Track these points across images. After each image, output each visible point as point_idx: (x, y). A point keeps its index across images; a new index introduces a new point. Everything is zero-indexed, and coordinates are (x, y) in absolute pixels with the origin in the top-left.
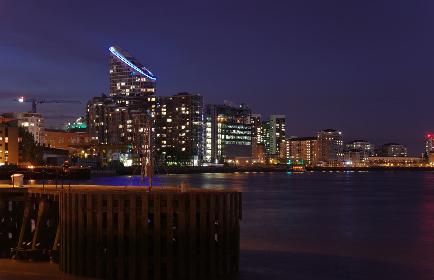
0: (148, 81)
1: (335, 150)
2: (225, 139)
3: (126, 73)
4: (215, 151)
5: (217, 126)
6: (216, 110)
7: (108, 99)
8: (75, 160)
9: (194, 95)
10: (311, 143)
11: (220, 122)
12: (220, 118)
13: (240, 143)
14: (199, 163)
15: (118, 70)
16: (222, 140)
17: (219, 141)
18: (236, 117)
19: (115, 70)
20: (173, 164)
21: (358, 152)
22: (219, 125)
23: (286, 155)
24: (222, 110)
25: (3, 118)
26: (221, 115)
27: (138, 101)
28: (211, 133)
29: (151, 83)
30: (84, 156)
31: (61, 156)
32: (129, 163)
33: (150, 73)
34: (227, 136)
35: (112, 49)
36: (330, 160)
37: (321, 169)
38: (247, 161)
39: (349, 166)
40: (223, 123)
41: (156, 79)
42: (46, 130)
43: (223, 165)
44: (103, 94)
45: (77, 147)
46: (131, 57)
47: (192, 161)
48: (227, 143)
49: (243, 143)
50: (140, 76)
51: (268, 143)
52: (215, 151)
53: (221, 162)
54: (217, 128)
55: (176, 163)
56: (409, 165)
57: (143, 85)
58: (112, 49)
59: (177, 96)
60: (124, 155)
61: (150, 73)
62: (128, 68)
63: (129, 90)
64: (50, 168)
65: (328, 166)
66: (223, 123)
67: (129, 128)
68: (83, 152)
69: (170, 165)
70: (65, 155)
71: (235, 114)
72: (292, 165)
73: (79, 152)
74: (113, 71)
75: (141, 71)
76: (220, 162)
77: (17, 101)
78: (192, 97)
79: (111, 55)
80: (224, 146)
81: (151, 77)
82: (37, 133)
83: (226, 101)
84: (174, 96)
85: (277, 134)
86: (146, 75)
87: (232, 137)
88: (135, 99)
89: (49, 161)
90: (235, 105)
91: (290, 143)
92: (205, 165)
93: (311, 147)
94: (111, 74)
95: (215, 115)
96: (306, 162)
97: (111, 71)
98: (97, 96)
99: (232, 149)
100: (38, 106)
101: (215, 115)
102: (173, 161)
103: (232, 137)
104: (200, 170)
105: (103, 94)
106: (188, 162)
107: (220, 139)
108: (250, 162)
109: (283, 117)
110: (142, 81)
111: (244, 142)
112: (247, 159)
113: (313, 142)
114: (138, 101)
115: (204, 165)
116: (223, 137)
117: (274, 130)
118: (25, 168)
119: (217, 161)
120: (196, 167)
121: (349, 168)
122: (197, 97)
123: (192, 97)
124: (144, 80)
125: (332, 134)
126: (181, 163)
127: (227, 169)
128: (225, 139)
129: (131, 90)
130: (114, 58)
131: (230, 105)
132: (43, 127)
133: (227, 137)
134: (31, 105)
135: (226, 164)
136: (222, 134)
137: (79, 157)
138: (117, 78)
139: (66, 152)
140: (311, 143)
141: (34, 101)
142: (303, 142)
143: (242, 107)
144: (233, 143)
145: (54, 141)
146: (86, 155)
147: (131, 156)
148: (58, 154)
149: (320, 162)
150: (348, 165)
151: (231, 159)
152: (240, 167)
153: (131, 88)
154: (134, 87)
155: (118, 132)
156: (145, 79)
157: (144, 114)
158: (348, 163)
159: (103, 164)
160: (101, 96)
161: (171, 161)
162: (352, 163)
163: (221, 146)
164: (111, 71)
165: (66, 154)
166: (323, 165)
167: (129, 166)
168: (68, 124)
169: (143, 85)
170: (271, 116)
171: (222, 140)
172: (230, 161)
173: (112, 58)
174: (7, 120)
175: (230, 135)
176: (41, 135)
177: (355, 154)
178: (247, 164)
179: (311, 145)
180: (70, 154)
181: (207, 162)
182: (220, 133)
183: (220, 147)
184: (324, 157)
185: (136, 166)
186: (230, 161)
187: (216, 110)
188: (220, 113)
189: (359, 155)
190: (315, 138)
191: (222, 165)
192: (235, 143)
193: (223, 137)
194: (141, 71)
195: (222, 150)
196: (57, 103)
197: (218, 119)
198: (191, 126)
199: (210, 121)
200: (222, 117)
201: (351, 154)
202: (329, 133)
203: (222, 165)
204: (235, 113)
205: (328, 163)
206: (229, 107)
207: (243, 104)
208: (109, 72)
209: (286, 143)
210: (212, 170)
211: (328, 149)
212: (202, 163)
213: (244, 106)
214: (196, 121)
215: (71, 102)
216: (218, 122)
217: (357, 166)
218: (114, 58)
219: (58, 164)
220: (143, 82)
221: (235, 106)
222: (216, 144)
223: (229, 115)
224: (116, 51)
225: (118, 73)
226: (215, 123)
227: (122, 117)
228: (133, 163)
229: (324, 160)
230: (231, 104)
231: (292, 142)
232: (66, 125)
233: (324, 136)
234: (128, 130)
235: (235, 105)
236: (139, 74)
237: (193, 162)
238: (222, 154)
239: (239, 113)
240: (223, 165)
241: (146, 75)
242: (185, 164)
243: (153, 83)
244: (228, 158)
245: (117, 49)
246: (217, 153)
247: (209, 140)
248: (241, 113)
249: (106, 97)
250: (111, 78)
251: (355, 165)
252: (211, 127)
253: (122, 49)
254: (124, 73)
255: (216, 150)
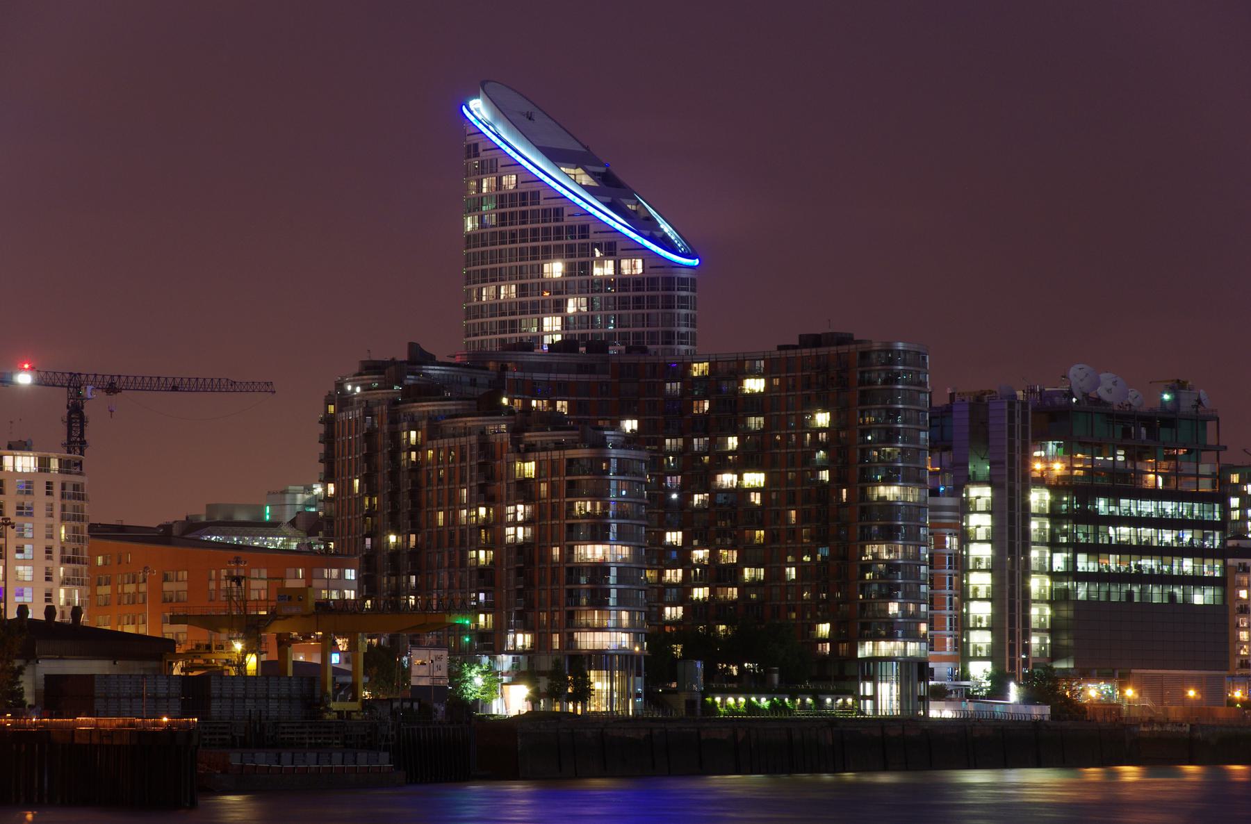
2: (1072, 573)
3: (546, 230)
4: (1012, 634)
5: (1026, 506)
6: (1018, 421)
7: (434, 370)
11: (1041, 482)
13: (1156, 594)
14: (903, 698)
15: (502, 219)
16: (1055, 576)
17: (1038, 585)
19: (491, 219)
20: (748, 704)
22: (1039, 498)
24: (1054, 419)
26: (1051, 446)
27: (593, 378)
29: (669, 283)
30: (242, 665)
31: (134, 668)
32: (514, 701)
33: (666, 228)
35: (478, 109)
38: (1192, 693)
40: (1057, 488)
41: (696, 262)
43: (1047, 710)
44: (413, 347)
45: (210, 622)
47: (868, 688)
49: (1172, 596)
52: (1012, 634)
54: (1027, 515)
55: (764, 703)
56: (558, 708)
58: (478, 109)
59: (791, 353)
60: (493, 658)
61: (666, 228)
63: (558, 320)
68: (238, 646)
69: (732, 712)
70: (153, 664)
73: (220, 647)
74: (481, 219)
76: (1029, 698)
79: (472, 140)
80: (1066, 612)
81: (674, 250)
83: (1077, 375)
87: (1112, 562)
90: (1133, 393)
92: (940, 711)
94: (472, 239)
97: (470, 224)
98: (378, 356)
99: (1098, 631)
102: (747, 692)
103: (1112, 562)
105: (413, 347)
106: (836, 694)
107: (1041, 571)
111: (1178, 591)
114: (593, 378)
115: (934, 713)
119: (1014, 693)
120: (889, 721)
123: (865, 355)
124: (633, 267)
126: (793, 699)
128: (1072, 573)
129: (566, 322)
131: (1102, 392)
134: (61, 398)
135: (1069, 710)
136: (1055, 546)
137: (220, 673)
139: (161, 649)
143: (1176, 400)
144: (1117, 593)
145: (143, 588)
146: (252, 662)
147: (524, 667)
148: (113, 656)
151: (1106, 677)
152: (1151, 721)
153: (571, 308)
156: (639, 263)
157: (582, 453)
160: (403, 356)
161: (736, 693)
164: (470, 224)
165: (159, 657)
167: (513, 712)
171: (1055, 576)
172: (1093, 691)
173: (477, 155)
175: (1095, 550)
176: (68, 561)
178: (1193, 705)
180: (178, 657)
183: (1039, 614)
186: (1093, 691)
187: (1018, 421)
191: (1040, 711)
192: (1130, 594)
193: (1059, 561)
194: (617, 223)
195: (1054, 629)
196: (175, 389)
197: (1038, 466)
198: (864, 510)
200: (1055, 458)
203: (1040, 711)
204: (1126, 433)
206: (1098, 401)
207: (1177, 387)
208: (462, 225)
212: (922, 698)
213: (1184, 394)
214: (888, 481)
219: (99, 704)
220: (628, 278)
221: (1135, 398)
222: (1019, 601)
223: (1094, 446)
224: (496, 118)
225: (502, 234)
226: (1012, 491)
227: (482, 466)
228: (534, 699)
230: (1108, 388)
232: (300, 498)
234: (510, 531)
237: (874, 698)
238: (1056, 653)
239: (1152, 434)
240: (1047, 710)
242: (819, 703)
243: (683, 281)
244: (1086, 673)
245: (501, 109)
246: (1027, 649)
247: (981, 581)
248: (1165, 434)
249: (430, 359)
250: (469, 261)
253: (527, 107)
254: (535, 231)
255: (1019, 630)
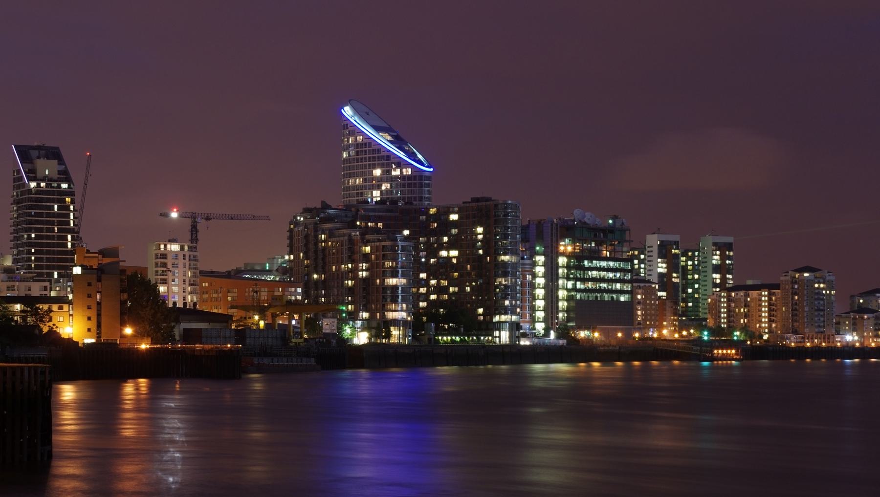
1: (819, 310)
4: (552, 313)
5: (558, 263)
7: (331, 211)
8: (241, 335)
9: (501, 202)
11: (563, 254)
12: (565, 246)
13: (606, 297)
14: (511, 337)
17: (562, 294)
18: (599, 244)
20: (452, 339)
21: (871, 315)
22: (562, 261)
23: (720, 322)
26: (567, 241)
27: (392, 214)
30: (258, 325)
31: (217, 326)
32: (362, 338)
33: (420, 156)
34: (578, 283)
35: (348, 111)
36: (807, 330)
37: (788, 352)
38: (620, 335)
39: (850, 345)
40: (569, 256)
41: (431, 170)
48: (578, 296)
49: (612, 298)
50: (400, 164)
51: (696, 296)
52: (552, 313)
55: (458, 339)
57: (407, 182)
58: (348, 111)
61: (420, 156)
62: (376, 147)
65: (802, 345)
66: (569, 256)
68: (257, 317)
69: (445, 342)
71: (597, 238)
72: (712, 345)
75: (401, 154)
76: (558, 337)
77: (166, 215)
79: (346, 122)
81: (422, 164)
83: (577, 213)
84: (462, 205)
85: (715, 276)
87: (590, 285)
89: (189, 336)
92: (524, 342)
93: (770, 305)
99: (587, 311)
100: (201, 224)
102: (451, 335)
103: (590, 285)
109: (730, 240)
110: (405, 173)
111: (615, 296)
112: (617, 331)
113: (774, 294)
114: (392, 214)
116: (570, 284)
117: (710, 269)
119: (553, 335)
120: (505, 346)
121: (849, 351)
122: (506, 206)
124: (408, 171)
125: (813, 278)
127: (573, 351)
129: (382, 193)
130: (350, 128)
131: (586, 220)
133: (579, 285)
134: (189, 221)
135: (576, 341)
137: (250, 328)
140: (770, 296)
141: (193, 216)
142: (754, 294)
143: (614, 222)
144: (592, 296)
148: (209, 321)
149: (788, 335)
152: (604, 345)
153: (383, 188)
154: (388, 185)
156: (410, 170)
158: (849, 338)
159: (294, 340)
160: (319, 206)
161: (447, 335)
162: (856, 338)
163: (566, 304)
165: (227, 322)
166: (792, 342)
167: (362, 343)
171: (568, 290)
172: (583, 334)
174: (106, 261)
175: (584, 280)
177: (863, 318)
179: (770, 299)
181: (537, 337)
183: (563, 305)
184: (796, 324)
185: (376, 344)
188: (563, 238)
190: (777, 287)
191: (562, 342)
192: (597, 297)
193: (570, 284)
194: (401, 154)
199: (543, 254)
201: (855, 318)
202: (806, 275)
203: (562, 342)
204: (595, 235)
205: (803, 338)
206: (585, 223)
207: (614, 218)
209: (720, 297)
210: (544, 353)
211: (804, 309)
214: (505, 254)
215: (254, 218)
216: (559, 254)
217: (866, 344)
218: (350, 128)
219: (204, 340)
221: (598, 222)
223: (583, 240)
225: (357, 159)
226: (552, 258)
229: (795, 332)
230: (589, 218)
231: (733, 294)
234: (360, 273)
237: (499, 337)
238: (569, 319)
239: (605, 236)
242: (479, 339)
243: (426, 177)
244: (580, 328)
245: (357, 111)
248: (610, 236)
251: (862, 344)
253: (367, 110)
254: (369, 158)
255: (554, 311)
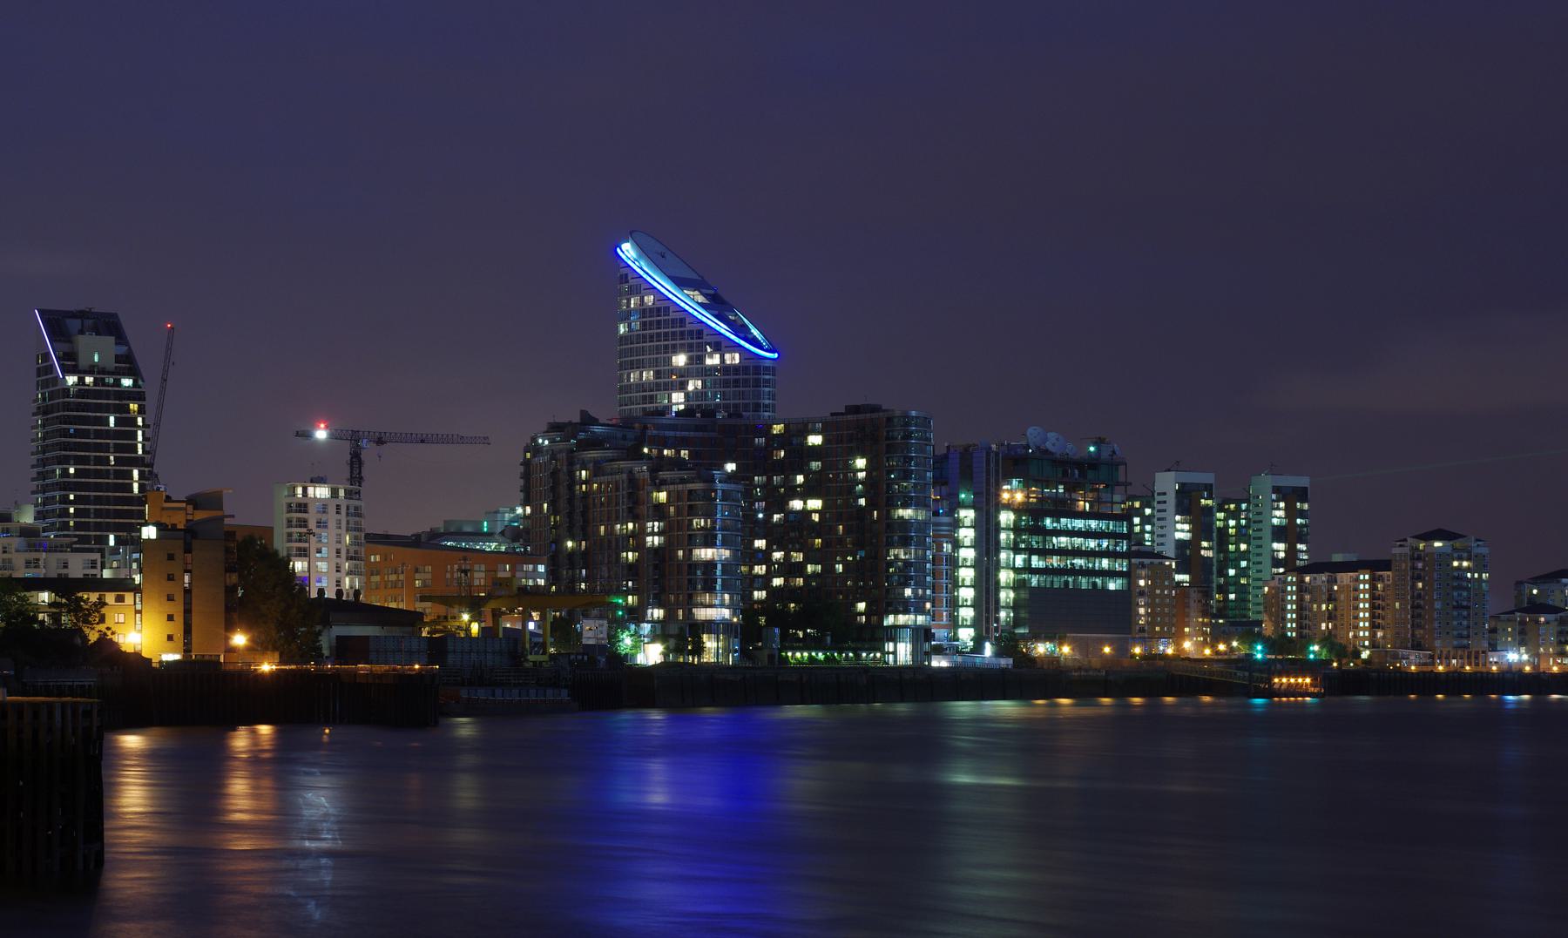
0: (747, 363)
1: (1459, 607)
2: (1028, 569)
3: (674, 333)
4: (988, 611)
7: (597, 429)
8: (438, 648)
9: (898, 413)
10: (1373, 582)
13: (1084, 582)
14: (914, 653)
15: (644, 325)
17: (1005, 576)
19: (636, 325)
20: (810, 657)
21: (1552, 617)
22: (1006, 518)
23: (1284, 627)
24: (1017, 464)
25: (190, 508)
26: (1015, 482)
27: (706, 435)
28: (976, 545)
29: (757, 370)
30: (468, 630)
31: (396, 631)
32: (652, 654)
33: (755, 332)
34: (1035, 559)
35: (628, 251)
36: (1438, 643)
38: (1107, 650)
40: (1019, 510)
42: (373, 539)
43: (1011, 661)
44: (584, 413)
46: (695, 276)
48: (1034, 581)
49: (1095, 584)
52: (988, 611)
53: (1007, 645)
54: (998, 528)
55: (821, 656)
58: (628, 251)
59: (840, 418)
61: (755, 332)
62: (678, 315)
63: (682, 395)
64: (355, 674)
65: (1430, 668)
66: (1019, 510)
67: (653, 534)
68: (466, 617)
69: (799, 662)
71: (1067, 477)
75: (722, 328)
76: (999, 653)
77: (307, 435)
78: (889, 420)
79: (624, 271)
81: (759, 346)
82: (338, 551)
85: (1276, 546)
86: (742, 343)
87: (1055, 561)
88: (698, 428)
90: (1070, 446)
91: (1300, 583)
92: (939, 662)
93: (1373, 598)
95: (988, 483)
96: (1345, 651)
97: (622, 329)
98: (562, 418)
99: (1049, 606)
100: (369, 451)
101: (988, 483)
102: (809, 649)
103: (1055, 561)
104: (918, 684)
105: (584, 413)
106: (869, 650)
107: (1008, 567)
108: (1122, 650)
109: (1303, 481)
113: (1381, 579)
114: (706, 435)
116: (1019, 560)
117: (1267, 534)
118: (249, 671)
121: (1513, 680)
122: (906, 420)
123: (889, 420)
124: (733, 359)
127: (1025, 679)
128: (1028, 569)
129: (687, 395)
131: (1048, 445)
132: (360, 530)
133: (1036, 562)
134: (346, 447)
135: (1030, 661)
136: (1016, 550)
137: (453, 635)
138: (643, 351)
140: (1373, 581)
142: (1344, 578)
143: (1098, 450)
144: (1058, 582)
146: (475, 628)
147: (659, 632)
148: (382, 623)
150: (1510, 665)
152: (1080, 669)
153: (691, 387)
155: (609, 547)
157: (698, 486)
158: (1512, 657)
160: (577, 419)
161: (802, 650)
162: (1525, 657)
163: (1012, 595)
165: (412, 625)
167: (651, 663)
168: (513, 510)
169: (732, 377)
170: (1254, 479)
171: (1016, 570)
172: (1042, 649)
174: (200, 515)
175: (1044, 553)
177: (1537, 622)
179: (1373, 588)
180: (426, 624)
182: (1008, 548)
183: (1006, 596)
184: (1419, 632)
189: (1554, 628)
190: (1386, 565)
191: (1006, 662)
192: (1067, 583)
193: (1019, 560)
194: (722, 328)
198: (888, 526)
201: (1523, 623)
202: (1438, 544)
203: (1006, 662)
204: (1065, 473)
205: (1432, 657)
206: (1046, 451)
208: (617, 329)
209: (1285, 583)
211: (1437, 605)
212: (926, 653)
213: (1104, 447)
214: (905, 506)
215: (462, 440)
217: (1543, 667)
221: (1070, 449)
222: (992, 588)
223: (1043, 482)
224: (639, 256)
226: (988, 513)
227: (630, 495)
229: (1417, 646)
230: (1053, 442)
231: (1307, 579)
233: (1416, 556)
235: (1070, 446)
236: (717, 339)
237: (895, 653)
238: (1017, 622)
239: (1083, 474)
240: (1011, 661)
241: (742, 343)
242: (858, 656)
243: (767, 368)
244: (1037, 637)
246: (997, 620)
248: (1091, 474)
249: (595, 422)
250: (622, 354)
251: (1535, 667)
252: (976, 525)
254: (666, 334)
255: (992, 607)
